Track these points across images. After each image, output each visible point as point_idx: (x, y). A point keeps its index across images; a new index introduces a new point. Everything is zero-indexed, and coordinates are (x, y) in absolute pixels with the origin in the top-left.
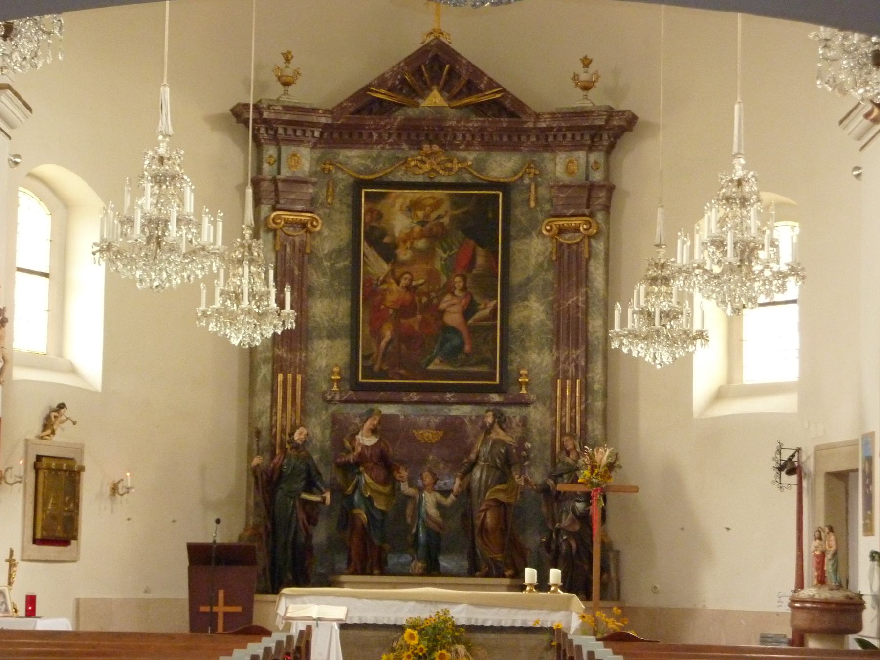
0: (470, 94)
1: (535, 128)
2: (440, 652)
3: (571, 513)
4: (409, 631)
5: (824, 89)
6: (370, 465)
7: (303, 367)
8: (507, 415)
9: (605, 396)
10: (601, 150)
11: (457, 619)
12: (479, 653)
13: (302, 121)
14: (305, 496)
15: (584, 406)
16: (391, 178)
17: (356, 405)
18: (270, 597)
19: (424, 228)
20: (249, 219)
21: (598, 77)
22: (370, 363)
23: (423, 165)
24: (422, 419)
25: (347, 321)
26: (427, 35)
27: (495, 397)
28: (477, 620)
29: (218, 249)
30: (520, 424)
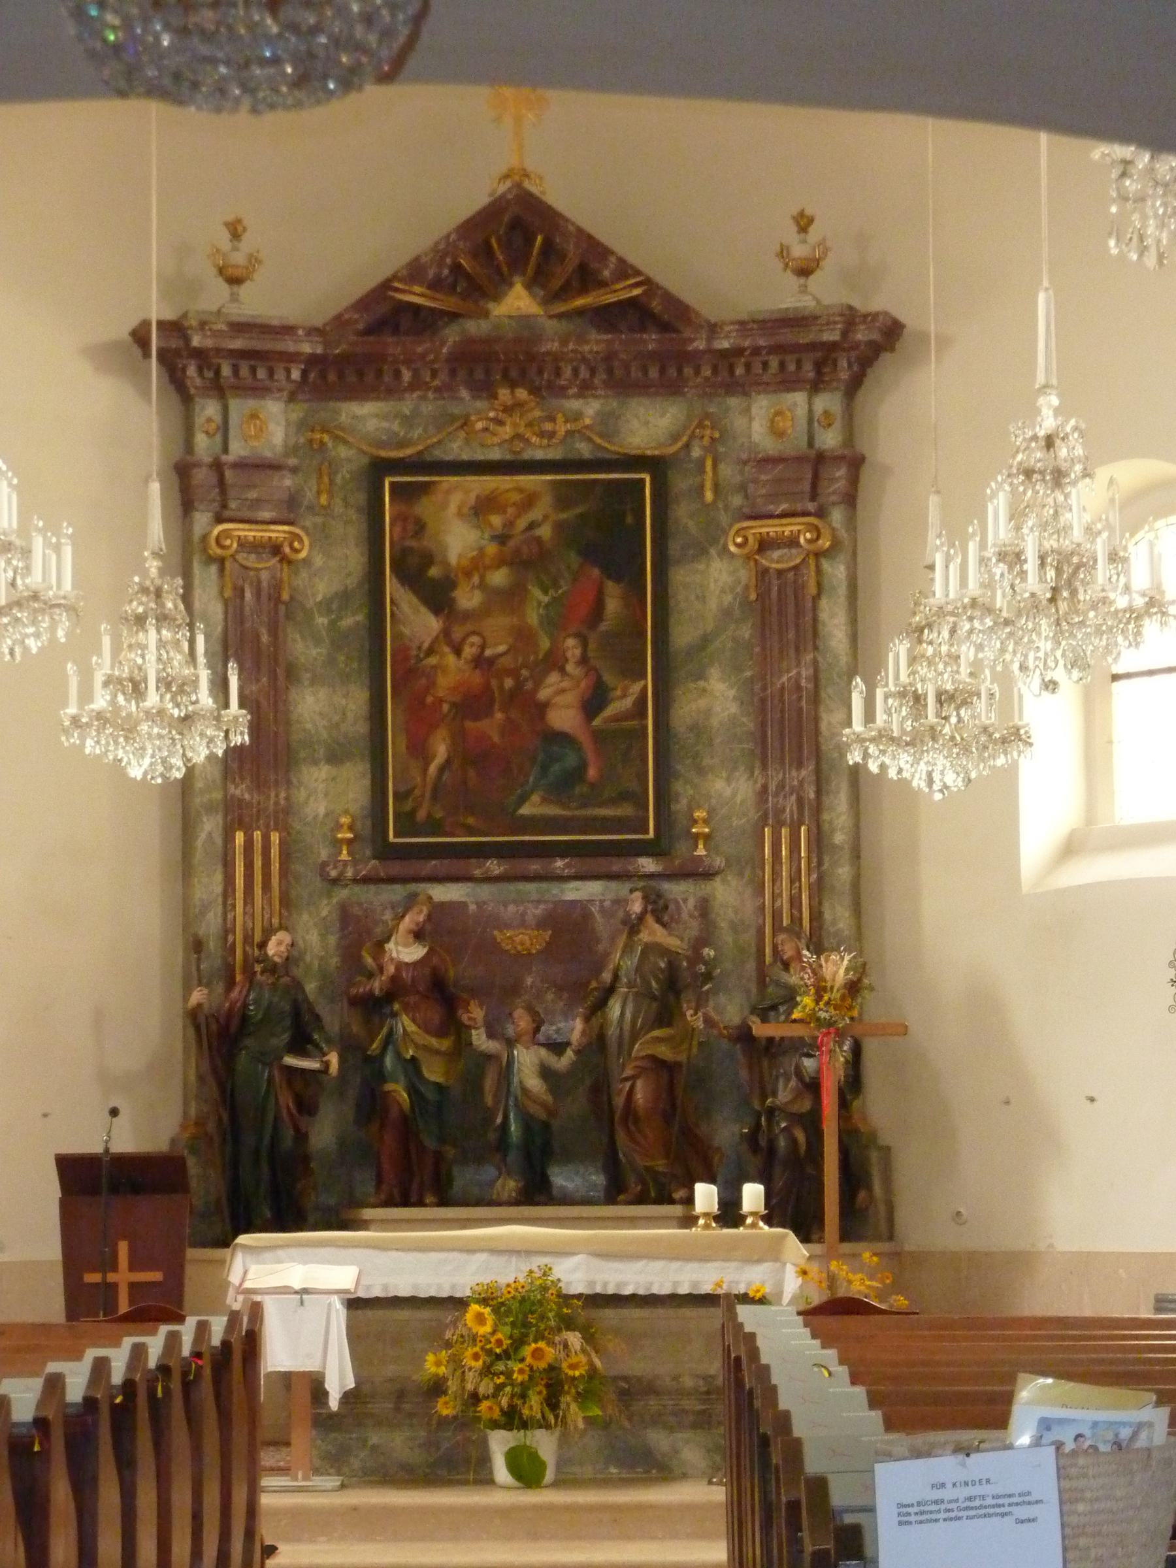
0: (584, 290)
1: (710, 351)
2: (533, 1345)
3: (794, 1078)
4: (475, 1308)
5: (1122, 257)
6: (412, 999)
7: (282, 818)
8: (672, 897)
9: (856, 855)
10: (837, 389)
11: (569, 1284)
12: (610, 1346)
13: (267, 352)
14: (290, 1061)
15: (815, 876)
16: (439, 454)
17: (383, 886)
18: (218, 1253)
19: (504, 549)
20: (156, 538)
21: (826, 250)
22: (408, 806)
23: (499, 429)
24: (511, 908)
25: (363, 728)
26: (500, 179)
27: (648, 864)
28: (605, 1284)
29: (65, 598)
30: (696, 914)
